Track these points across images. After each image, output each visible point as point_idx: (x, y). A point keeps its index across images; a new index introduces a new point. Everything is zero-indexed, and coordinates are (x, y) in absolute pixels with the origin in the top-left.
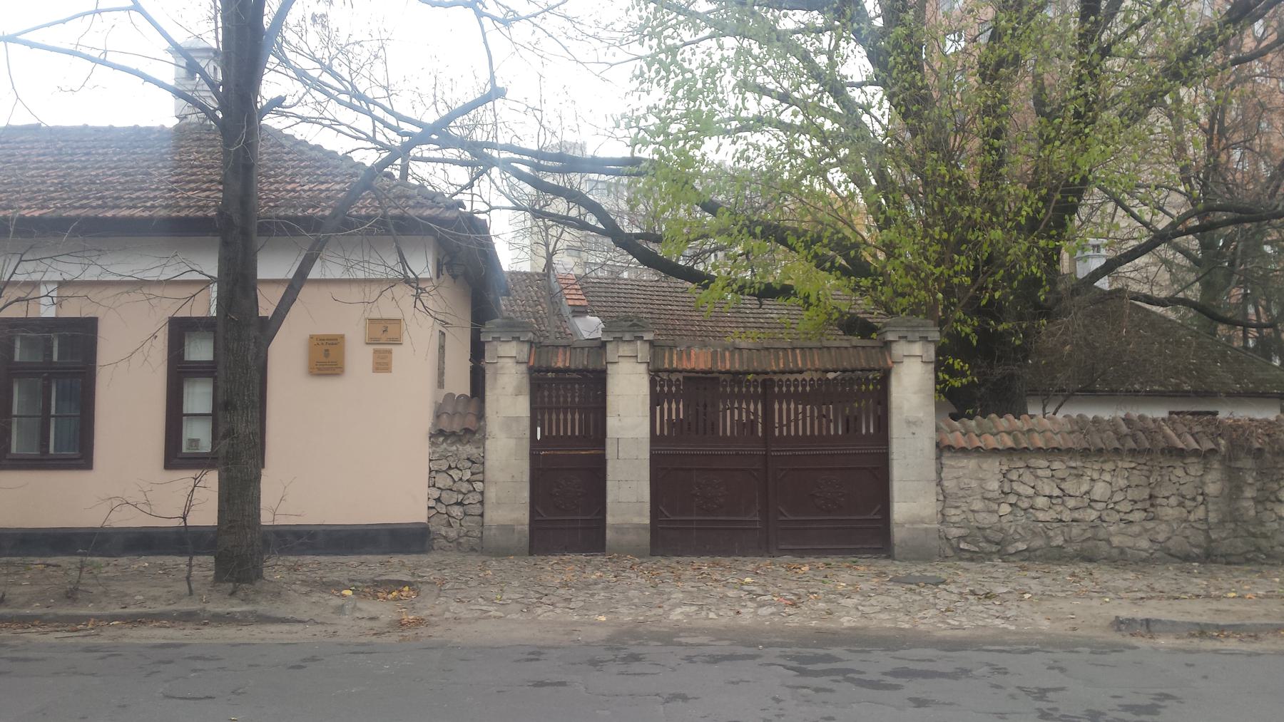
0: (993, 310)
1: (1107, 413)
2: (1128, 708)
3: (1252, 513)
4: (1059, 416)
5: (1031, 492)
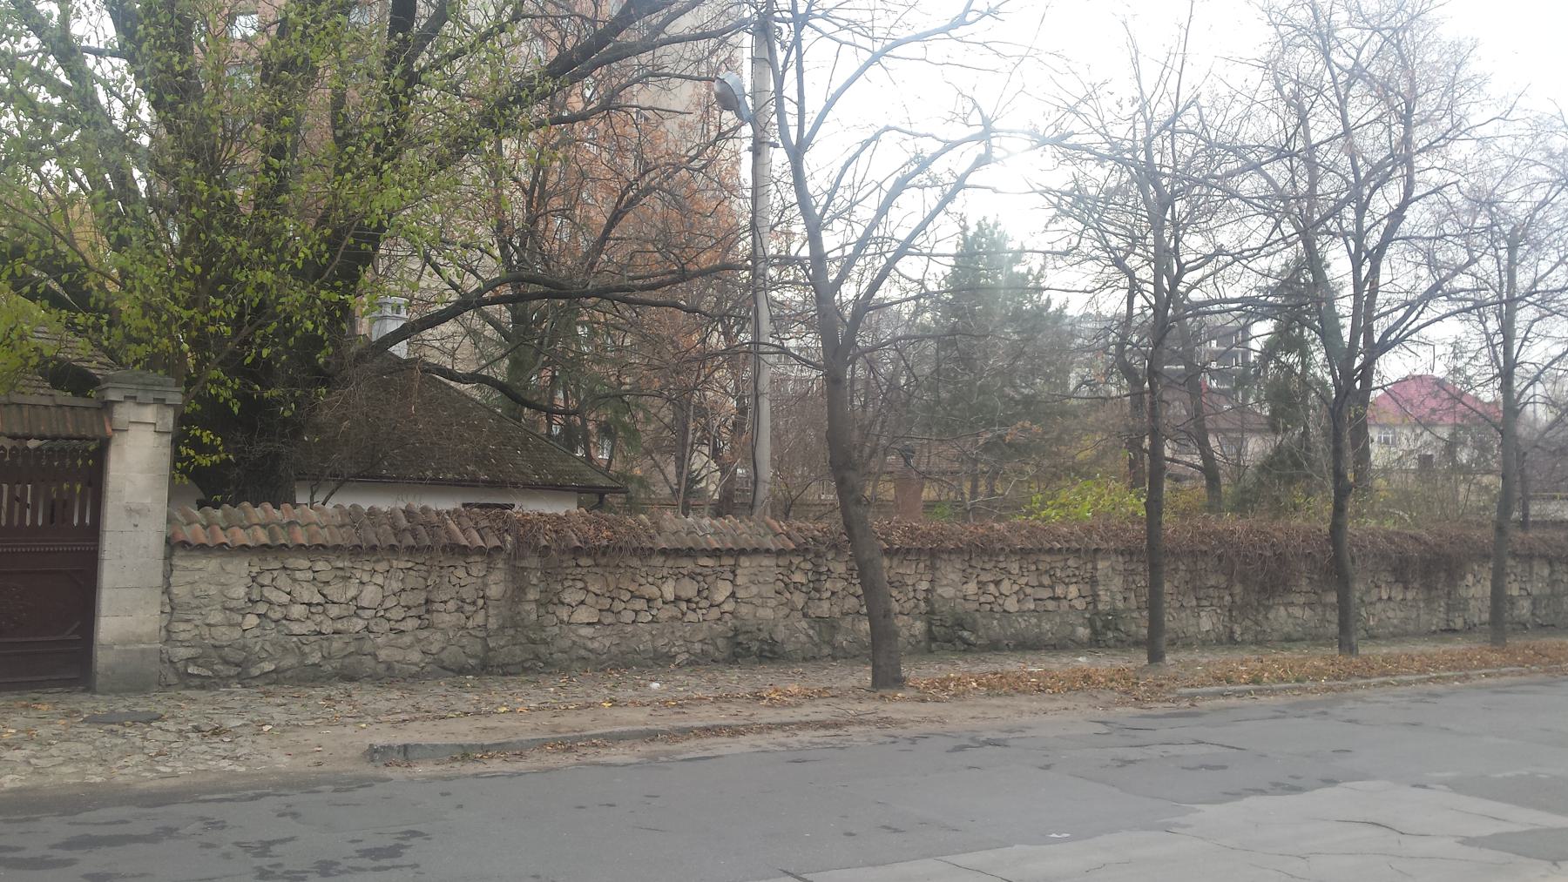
0: (261, 372)
1: (385, 503)
2: (366, 853)
3: (534, 617)
4: (329, 506)
5: (285, 599)
